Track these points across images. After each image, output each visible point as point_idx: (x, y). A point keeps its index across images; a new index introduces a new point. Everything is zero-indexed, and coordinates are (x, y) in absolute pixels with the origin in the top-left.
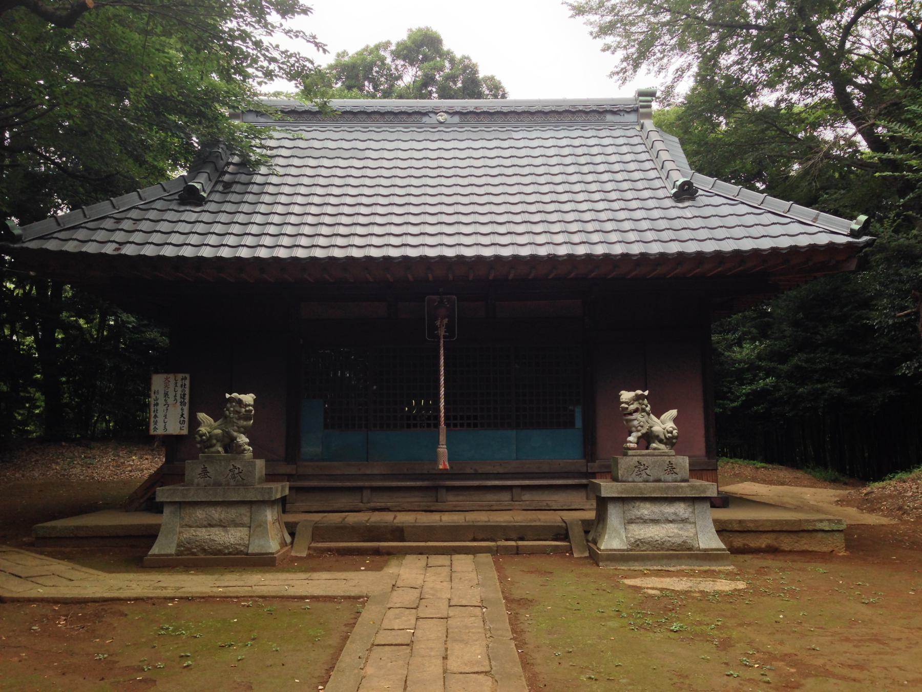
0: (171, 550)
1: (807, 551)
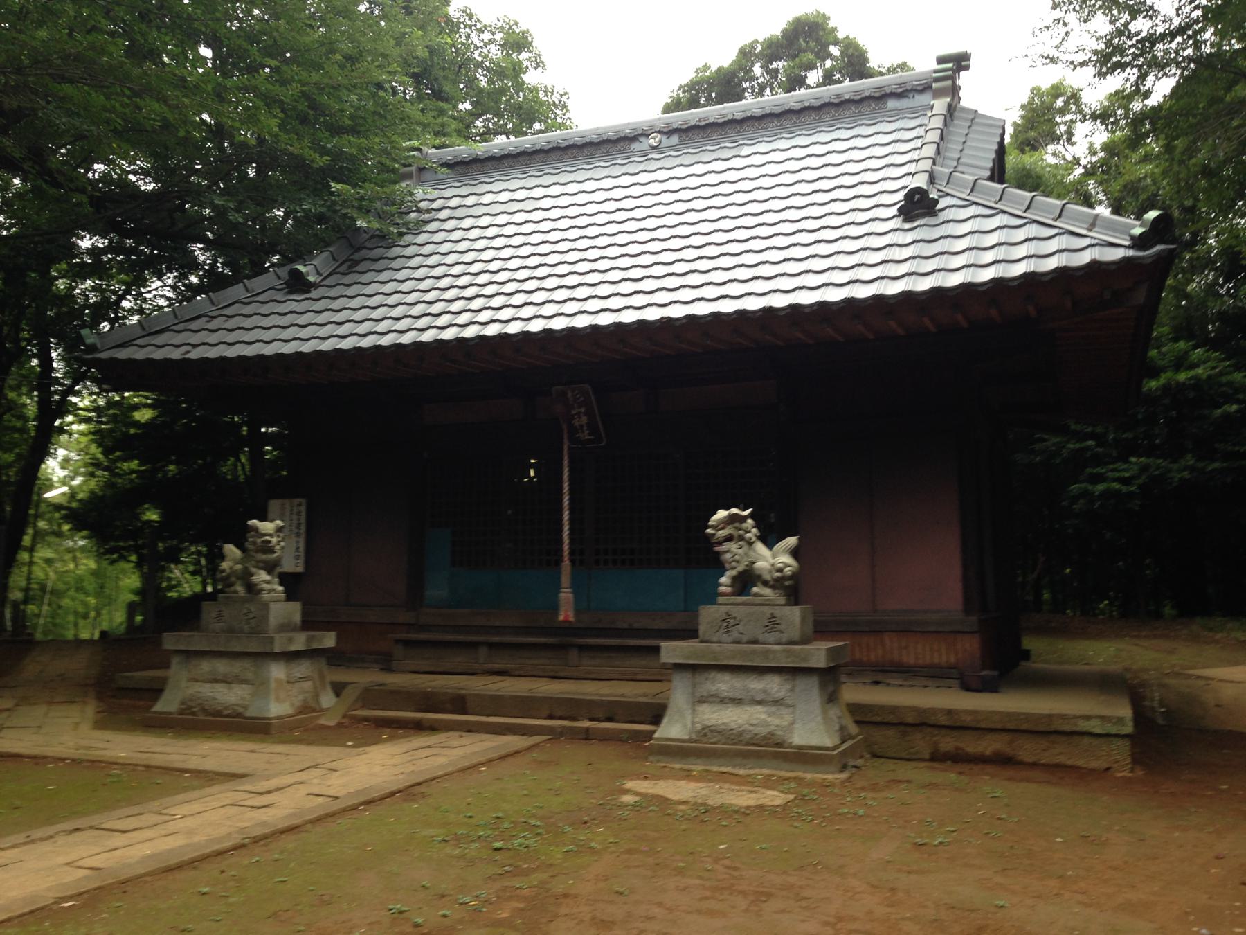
1: (1066, 766)
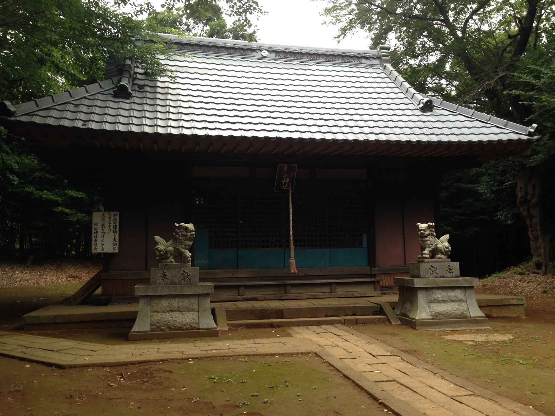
0: (147, 328)
1: (506, 317)
